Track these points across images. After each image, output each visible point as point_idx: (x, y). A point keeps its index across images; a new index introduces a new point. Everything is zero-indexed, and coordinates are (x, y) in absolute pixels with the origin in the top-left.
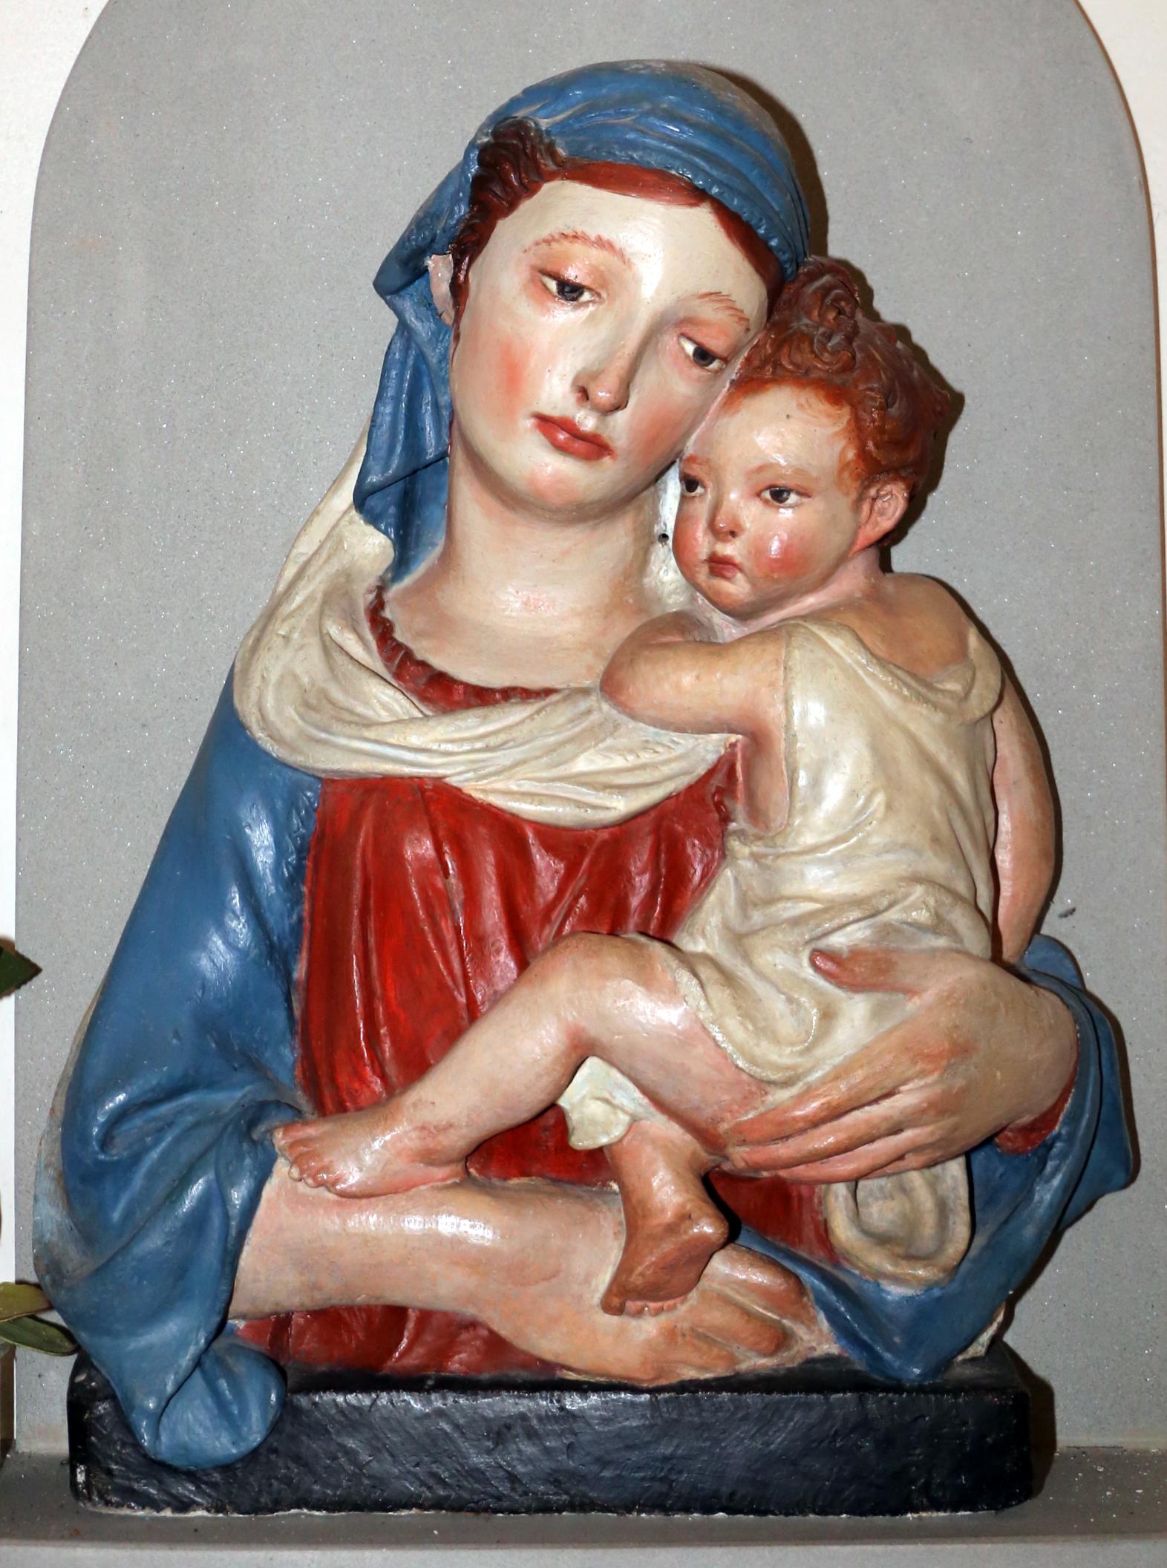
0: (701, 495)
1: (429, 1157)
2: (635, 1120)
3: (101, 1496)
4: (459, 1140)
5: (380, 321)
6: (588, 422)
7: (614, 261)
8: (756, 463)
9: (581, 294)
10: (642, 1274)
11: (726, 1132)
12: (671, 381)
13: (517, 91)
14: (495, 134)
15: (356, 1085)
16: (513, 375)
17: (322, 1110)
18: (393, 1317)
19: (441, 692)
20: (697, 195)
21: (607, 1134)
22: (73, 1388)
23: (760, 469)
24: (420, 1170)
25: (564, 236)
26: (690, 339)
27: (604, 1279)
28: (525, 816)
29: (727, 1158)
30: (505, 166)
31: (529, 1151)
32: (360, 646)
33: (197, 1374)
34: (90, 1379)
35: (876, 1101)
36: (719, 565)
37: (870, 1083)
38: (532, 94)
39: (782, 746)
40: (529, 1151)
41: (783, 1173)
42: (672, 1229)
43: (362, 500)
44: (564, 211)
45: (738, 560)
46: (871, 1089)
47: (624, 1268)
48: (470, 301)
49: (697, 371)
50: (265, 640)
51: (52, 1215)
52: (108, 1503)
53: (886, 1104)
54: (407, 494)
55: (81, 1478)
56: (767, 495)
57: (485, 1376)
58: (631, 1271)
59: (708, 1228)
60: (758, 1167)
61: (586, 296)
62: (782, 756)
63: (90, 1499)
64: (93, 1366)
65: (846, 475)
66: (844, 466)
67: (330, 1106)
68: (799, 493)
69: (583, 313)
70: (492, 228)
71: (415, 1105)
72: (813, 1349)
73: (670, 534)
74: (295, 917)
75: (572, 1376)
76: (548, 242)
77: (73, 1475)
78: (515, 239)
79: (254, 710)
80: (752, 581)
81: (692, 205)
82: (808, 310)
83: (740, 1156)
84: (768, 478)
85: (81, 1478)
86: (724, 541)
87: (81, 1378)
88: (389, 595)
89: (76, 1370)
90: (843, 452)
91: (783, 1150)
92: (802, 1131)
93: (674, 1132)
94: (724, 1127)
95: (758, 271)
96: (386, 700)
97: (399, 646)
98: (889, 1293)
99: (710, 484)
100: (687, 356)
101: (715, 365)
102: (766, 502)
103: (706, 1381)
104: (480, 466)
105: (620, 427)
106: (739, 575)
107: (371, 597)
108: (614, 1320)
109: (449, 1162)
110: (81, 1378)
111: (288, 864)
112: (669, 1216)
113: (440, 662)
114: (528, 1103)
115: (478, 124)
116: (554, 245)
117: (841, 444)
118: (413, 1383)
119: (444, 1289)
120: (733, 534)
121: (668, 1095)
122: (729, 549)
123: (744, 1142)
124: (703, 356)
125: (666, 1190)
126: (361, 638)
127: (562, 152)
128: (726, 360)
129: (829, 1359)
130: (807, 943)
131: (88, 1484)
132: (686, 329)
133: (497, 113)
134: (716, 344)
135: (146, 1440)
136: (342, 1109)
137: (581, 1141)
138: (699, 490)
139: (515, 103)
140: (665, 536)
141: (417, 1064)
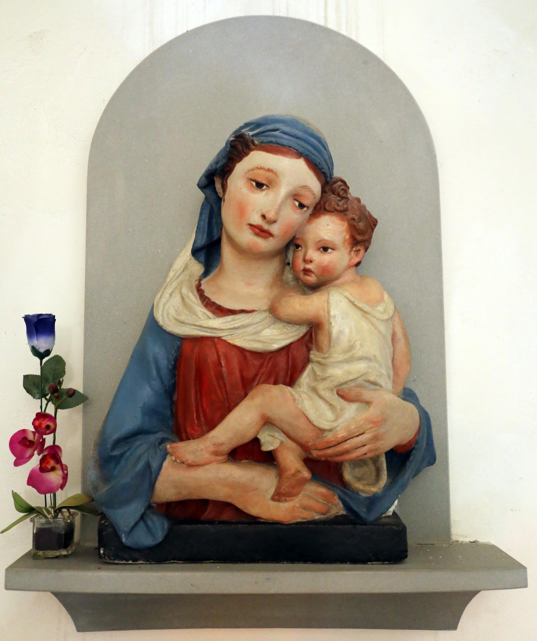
0: (301, 250)
1: (216, 453)
2: (282, 442)
3: (109, 557)
4: (227, 448)
5: (200, 196)
6: (266, 227)
7: (274, 175)
8: (318, 240)
9: (263, 186)
10: (284, 489)
11: (311, 445)
12: (292, 216)
13: (242, 124)
14: (236, 137)
15: (193, 432)
16: (242, 211)
17: (182, 440)
18: (204, 503)
19: (220, 311)
20: (299, 155)
21: (272, 446)
22: (100, 525)
23: (319, 241)
24: (213, 458)
25: (258, 168)
26: (297, 201)
27: (272, 491)
28: (246, 349)
29: (311, 454)
30: (238, 147)
31: (249, 452)
32: (194, 299)
33: (142, 524)
34: (105, 522)
35: (358, 436)
36: (307, 271)
37: (356, 430)
38: (247, 125)
39: (326, 327)
40: (249, 452)
41: (329, 459)
42: (293, 475)
43: (195, 252)
44: (257, 159)
45: (313, 270)
46: (356, 432)
47: (278, 487)
48: (228, 189)
49: (299, 211)
50: (164, 295)
51: (93, 474)
52: (111, 559)
53: (361, 437)
54: (209, 251)
55: (102, 552)
56: (322, 249)
57: (234, 521)
58: (280, 488)
59: (306, 474)
60: (321, 456)
61: (265, 187)
62: (322, 516)
63: (105, 558)
64: (106, 518)
65: (346, 243)
66: (345, 241)
67: (184, 437)
68: (331, 249)
69: (264, 193)
70: (234, 167)
71: (212, 437)
72: (338, 513)
73: (291, 262)
74: (173, 381)
75: (262, 521)
76: (252, 170)
77: (99, 551)
78: (242, 168)
79: (161, 317)
80: (317, 276)
81: (298, 158)
82: (332, 195)
83: (315, 454)
84: (322, 244)
85: (102, 552)
86: (308, 264)
87: (103, 522)
88: (203, 282)
89: (101, 520)
90: (345, 237)
91: (330, 451)
92: (335, 446)
93: (293, 445)
94: (310, 444)
95: (318, 179)
96: (200, 309)
97: (206, 297)
98: (361, 496)
99: (303, 246)
100: (296, 206)
101: (305, 209)
102: (321, 252)
103: (305, 522)
104: (231, 240)
105: (274, 229)
106: (313, 275)
107: (197, 282)
108: (276, 503)
109: (223, 455)
110: (103, 522)
111: (171, 364)
112: (292, 472)
113: (219, 302)
114: (249, 436)
115: (230, 134)
116: (255, 171)
117: (344, 234)
118: (211, 522)
119: (221, 494)
120: (311, 262)
121: (293, 434)
122: (309, 266)
123: (316, 449)
124: (301, 206)
125: (291, 460)
126: (194, 294)
127: (256, 142)
128: (308, 208)
129: (343, 516)
130: (335, 387)
131: (104, 553)
132: (296, 198)
133: (236, 132)
134: (305, 202)
135: (124, 540)
136: (188, 439)
137: (266, 448)
138: (300, 248)
139: (242, 128)
140: (289, 264)
141: (212, 425)
